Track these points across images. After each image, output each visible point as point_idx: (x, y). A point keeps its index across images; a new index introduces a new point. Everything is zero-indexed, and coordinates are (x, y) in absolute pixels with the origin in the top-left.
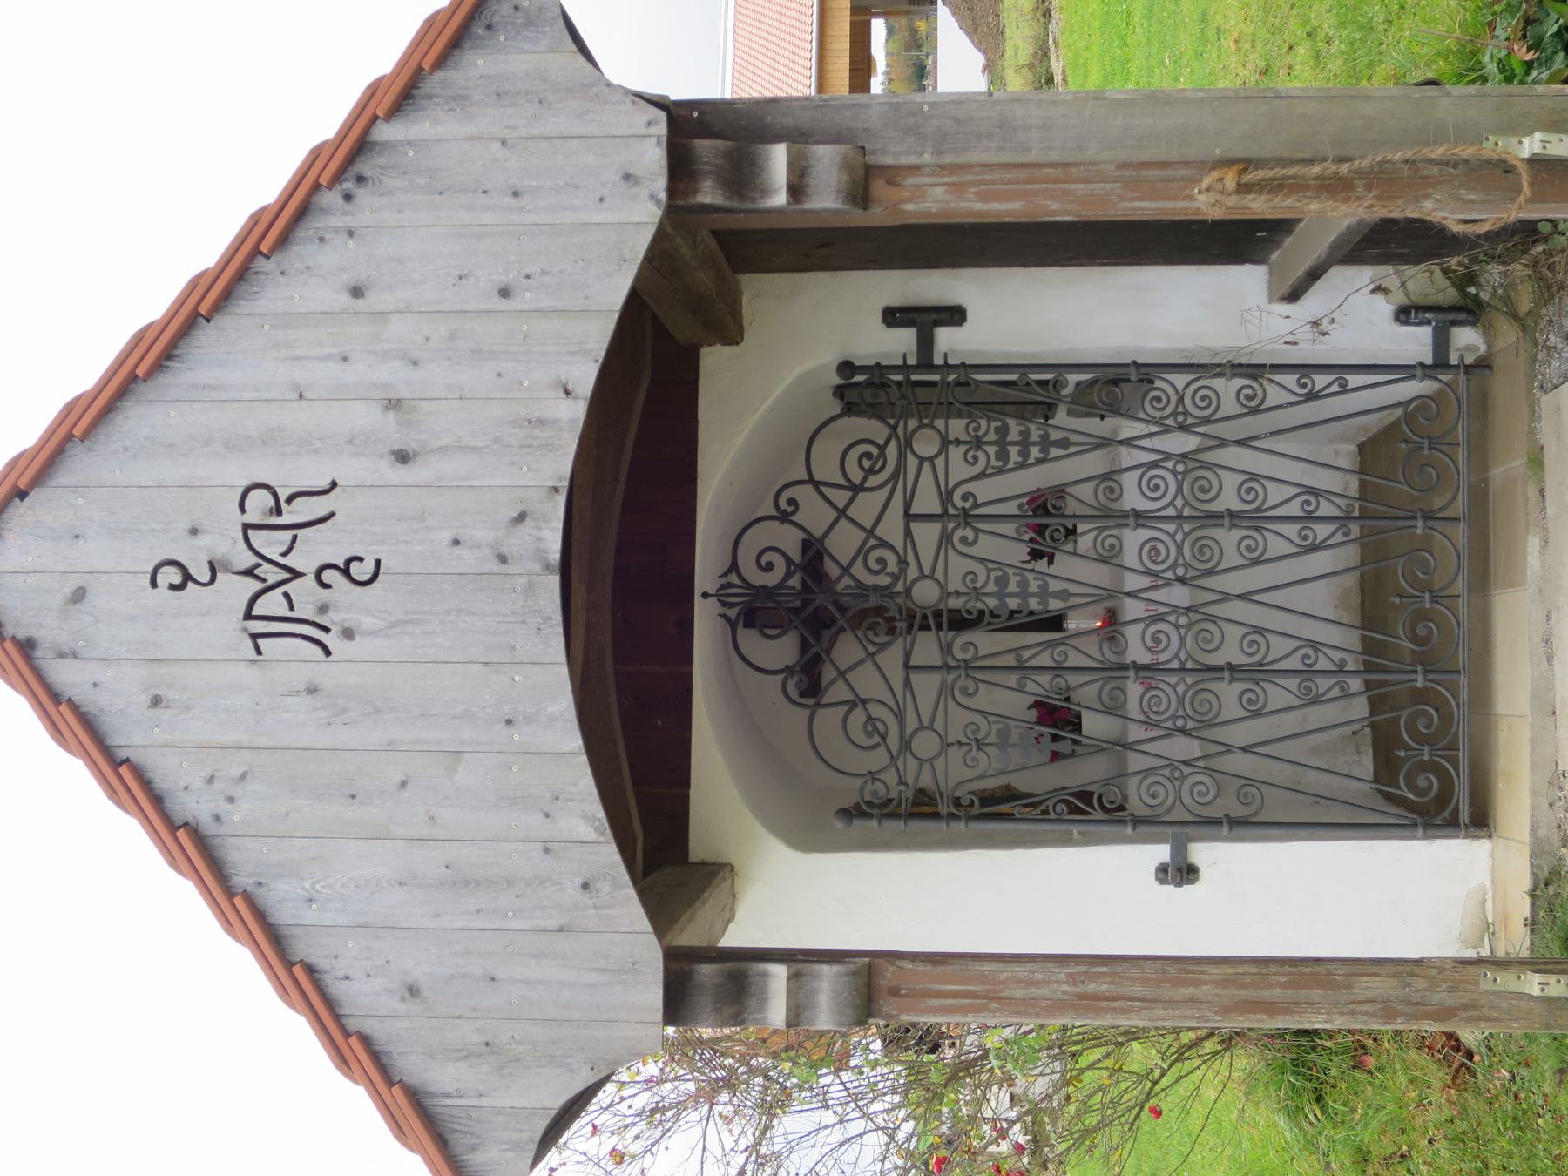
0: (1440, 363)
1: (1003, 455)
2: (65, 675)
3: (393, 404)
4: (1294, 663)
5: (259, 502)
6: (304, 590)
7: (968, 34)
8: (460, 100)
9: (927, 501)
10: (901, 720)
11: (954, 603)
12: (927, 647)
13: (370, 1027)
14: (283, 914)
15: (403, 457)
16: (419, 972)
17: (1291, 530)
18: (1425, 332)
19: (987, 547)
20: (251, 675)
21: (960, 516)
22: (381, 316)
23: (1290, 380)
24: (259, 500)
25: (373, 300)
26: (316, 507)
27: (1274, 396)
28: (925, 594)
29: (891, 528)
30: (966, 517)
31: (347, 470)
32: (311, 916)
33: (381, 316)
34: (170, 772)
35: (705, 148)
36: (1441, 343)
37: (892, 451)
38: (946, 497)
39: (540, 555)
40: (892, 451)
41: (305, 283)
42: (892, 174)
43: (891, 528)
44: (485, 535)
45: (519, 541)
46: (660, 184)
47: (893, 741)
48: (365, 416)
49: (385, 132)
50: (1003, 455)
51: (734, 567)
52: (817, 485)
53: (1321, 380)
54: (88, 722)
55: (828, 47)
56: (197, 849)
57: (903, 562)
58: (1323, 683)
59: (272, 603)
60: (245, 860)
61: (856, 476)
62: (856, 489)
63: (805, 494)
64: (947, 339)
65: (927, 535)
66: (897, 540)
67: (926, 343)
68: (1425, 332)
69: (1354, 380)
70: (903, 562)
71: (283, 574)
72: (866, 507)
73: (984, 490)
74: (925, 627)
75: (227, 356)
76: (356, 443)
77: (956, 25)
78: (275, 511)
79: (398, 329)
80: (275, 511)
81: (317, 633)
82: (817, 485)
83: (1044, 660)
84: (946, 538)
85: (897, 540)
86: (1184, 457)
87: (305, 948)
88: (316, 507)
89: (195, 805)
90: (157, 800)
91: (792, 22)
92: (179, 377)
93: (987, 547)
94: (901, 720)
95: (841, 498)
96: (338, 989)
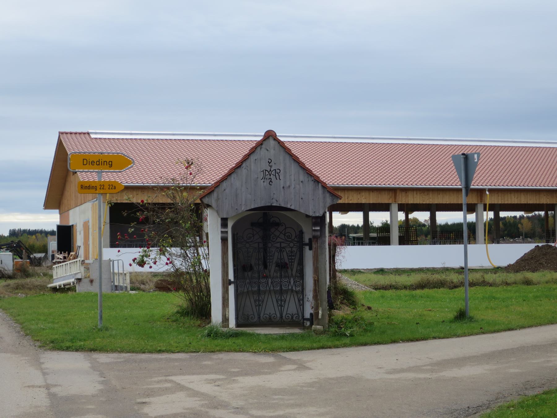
0: (304, 319)
1: (290, 256)
2: (259, 149)
3: (289, 186)
4: (260, 299)
5: (278, 171)
6: (268, 177)
7: (522, 257)
8: (324, 193)
9: (283, 245)
10: (251, 242)
11: (268, 249)
12: (261, 245)
13: (220, 186)
14: (233, 175)
15: (283, 187)
16: (227, 191)
17: (280, 298)
18: (309, 317)
19: (276, 254)
20: (259, 170)
21: (281, 250)
22: (299, 185)
23: (301, 297)
24: (278, 171)
25: (301, 184)
26: (278, 178)
27: (299, 295)
28: (270, 245)
29: (279, 240)
30: (281, 251)
31: (282, 182)
32: (232, 178)
33: (299, 185)
34: (248, 162)
35: (319, 220)
36: (307, 319)
37: (290, 240)
38: (284, 248)
39: (273, 203)
40: (290, 240)
41: (302, 176)
42: (317, 241)
43: (279, 240)
44: (275, 196)
45: (274, 201)
46: (314, 215)
47: (248, 241)
48: (288, 184)
49: (320, 185)
50: (290, 256)
51: (273, 217)
52: (285, 229)
53: (301, 302)
54: (254, 152)
55: (522, 194)
56: (239, 166)
57: (274, 242)
58: (257, 303)
59: (267, 173)
60: (239, 170)
61: (287, 235)
62: (285, 235)
63: (284, 227)
64: (307, 248)
65: (278, 245)
66: (277, 241)
67: (306, 245)
68: (309, 317)
69: (302, 307)
70: (274, 242)
71: (271, 174)
72: (282, 236)
73: (285, 254)
74: (264, 245)
75: (293, 168)
76: (285, 182)
77: (527, 252)
78: (277, 173)
79: (298, 186)
80: (277, 173)
81: (264, 178)
82: (285, 229)
83: (260, 262)
84: (278, 248)
85: (277, 241)
86: (290, 282)
87: (229, 178)
88: (278, 178)
89: (244, 165)
90: (245, 160)
91: (550, 170)
92: (292, 161)
93: (276, 254)
94: (251, 242)
95: (283, 232)
96: (225, 182)
